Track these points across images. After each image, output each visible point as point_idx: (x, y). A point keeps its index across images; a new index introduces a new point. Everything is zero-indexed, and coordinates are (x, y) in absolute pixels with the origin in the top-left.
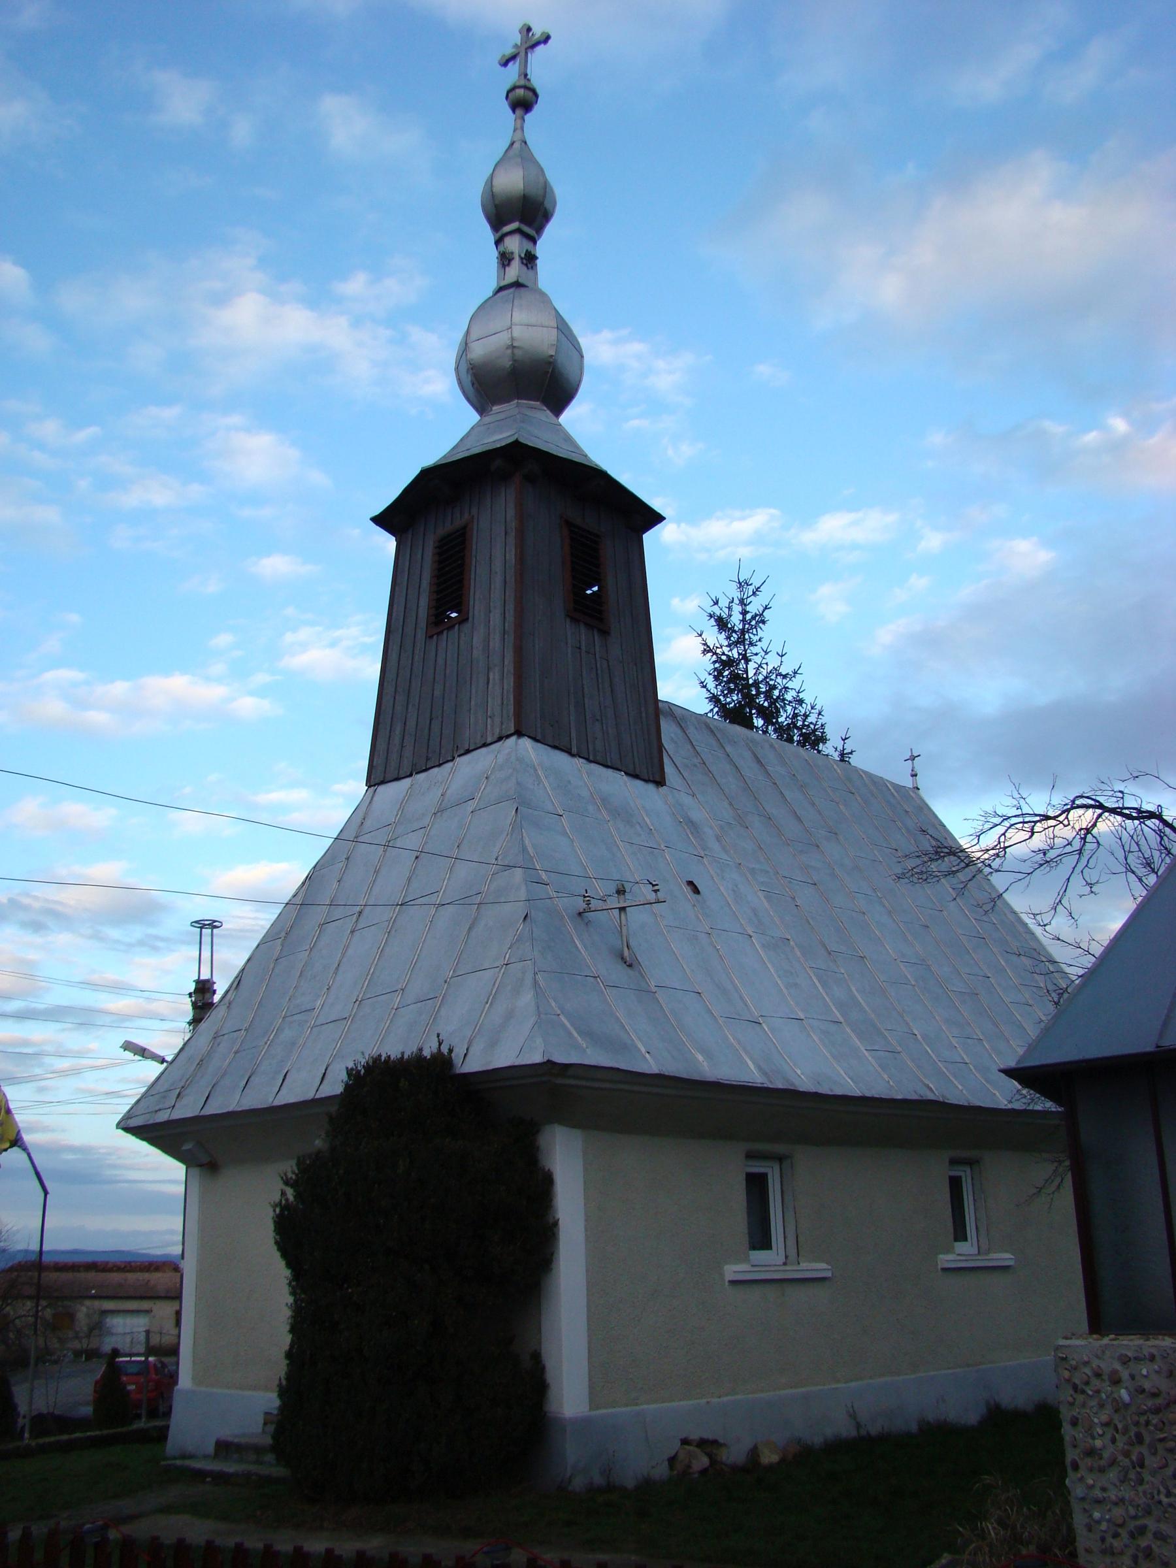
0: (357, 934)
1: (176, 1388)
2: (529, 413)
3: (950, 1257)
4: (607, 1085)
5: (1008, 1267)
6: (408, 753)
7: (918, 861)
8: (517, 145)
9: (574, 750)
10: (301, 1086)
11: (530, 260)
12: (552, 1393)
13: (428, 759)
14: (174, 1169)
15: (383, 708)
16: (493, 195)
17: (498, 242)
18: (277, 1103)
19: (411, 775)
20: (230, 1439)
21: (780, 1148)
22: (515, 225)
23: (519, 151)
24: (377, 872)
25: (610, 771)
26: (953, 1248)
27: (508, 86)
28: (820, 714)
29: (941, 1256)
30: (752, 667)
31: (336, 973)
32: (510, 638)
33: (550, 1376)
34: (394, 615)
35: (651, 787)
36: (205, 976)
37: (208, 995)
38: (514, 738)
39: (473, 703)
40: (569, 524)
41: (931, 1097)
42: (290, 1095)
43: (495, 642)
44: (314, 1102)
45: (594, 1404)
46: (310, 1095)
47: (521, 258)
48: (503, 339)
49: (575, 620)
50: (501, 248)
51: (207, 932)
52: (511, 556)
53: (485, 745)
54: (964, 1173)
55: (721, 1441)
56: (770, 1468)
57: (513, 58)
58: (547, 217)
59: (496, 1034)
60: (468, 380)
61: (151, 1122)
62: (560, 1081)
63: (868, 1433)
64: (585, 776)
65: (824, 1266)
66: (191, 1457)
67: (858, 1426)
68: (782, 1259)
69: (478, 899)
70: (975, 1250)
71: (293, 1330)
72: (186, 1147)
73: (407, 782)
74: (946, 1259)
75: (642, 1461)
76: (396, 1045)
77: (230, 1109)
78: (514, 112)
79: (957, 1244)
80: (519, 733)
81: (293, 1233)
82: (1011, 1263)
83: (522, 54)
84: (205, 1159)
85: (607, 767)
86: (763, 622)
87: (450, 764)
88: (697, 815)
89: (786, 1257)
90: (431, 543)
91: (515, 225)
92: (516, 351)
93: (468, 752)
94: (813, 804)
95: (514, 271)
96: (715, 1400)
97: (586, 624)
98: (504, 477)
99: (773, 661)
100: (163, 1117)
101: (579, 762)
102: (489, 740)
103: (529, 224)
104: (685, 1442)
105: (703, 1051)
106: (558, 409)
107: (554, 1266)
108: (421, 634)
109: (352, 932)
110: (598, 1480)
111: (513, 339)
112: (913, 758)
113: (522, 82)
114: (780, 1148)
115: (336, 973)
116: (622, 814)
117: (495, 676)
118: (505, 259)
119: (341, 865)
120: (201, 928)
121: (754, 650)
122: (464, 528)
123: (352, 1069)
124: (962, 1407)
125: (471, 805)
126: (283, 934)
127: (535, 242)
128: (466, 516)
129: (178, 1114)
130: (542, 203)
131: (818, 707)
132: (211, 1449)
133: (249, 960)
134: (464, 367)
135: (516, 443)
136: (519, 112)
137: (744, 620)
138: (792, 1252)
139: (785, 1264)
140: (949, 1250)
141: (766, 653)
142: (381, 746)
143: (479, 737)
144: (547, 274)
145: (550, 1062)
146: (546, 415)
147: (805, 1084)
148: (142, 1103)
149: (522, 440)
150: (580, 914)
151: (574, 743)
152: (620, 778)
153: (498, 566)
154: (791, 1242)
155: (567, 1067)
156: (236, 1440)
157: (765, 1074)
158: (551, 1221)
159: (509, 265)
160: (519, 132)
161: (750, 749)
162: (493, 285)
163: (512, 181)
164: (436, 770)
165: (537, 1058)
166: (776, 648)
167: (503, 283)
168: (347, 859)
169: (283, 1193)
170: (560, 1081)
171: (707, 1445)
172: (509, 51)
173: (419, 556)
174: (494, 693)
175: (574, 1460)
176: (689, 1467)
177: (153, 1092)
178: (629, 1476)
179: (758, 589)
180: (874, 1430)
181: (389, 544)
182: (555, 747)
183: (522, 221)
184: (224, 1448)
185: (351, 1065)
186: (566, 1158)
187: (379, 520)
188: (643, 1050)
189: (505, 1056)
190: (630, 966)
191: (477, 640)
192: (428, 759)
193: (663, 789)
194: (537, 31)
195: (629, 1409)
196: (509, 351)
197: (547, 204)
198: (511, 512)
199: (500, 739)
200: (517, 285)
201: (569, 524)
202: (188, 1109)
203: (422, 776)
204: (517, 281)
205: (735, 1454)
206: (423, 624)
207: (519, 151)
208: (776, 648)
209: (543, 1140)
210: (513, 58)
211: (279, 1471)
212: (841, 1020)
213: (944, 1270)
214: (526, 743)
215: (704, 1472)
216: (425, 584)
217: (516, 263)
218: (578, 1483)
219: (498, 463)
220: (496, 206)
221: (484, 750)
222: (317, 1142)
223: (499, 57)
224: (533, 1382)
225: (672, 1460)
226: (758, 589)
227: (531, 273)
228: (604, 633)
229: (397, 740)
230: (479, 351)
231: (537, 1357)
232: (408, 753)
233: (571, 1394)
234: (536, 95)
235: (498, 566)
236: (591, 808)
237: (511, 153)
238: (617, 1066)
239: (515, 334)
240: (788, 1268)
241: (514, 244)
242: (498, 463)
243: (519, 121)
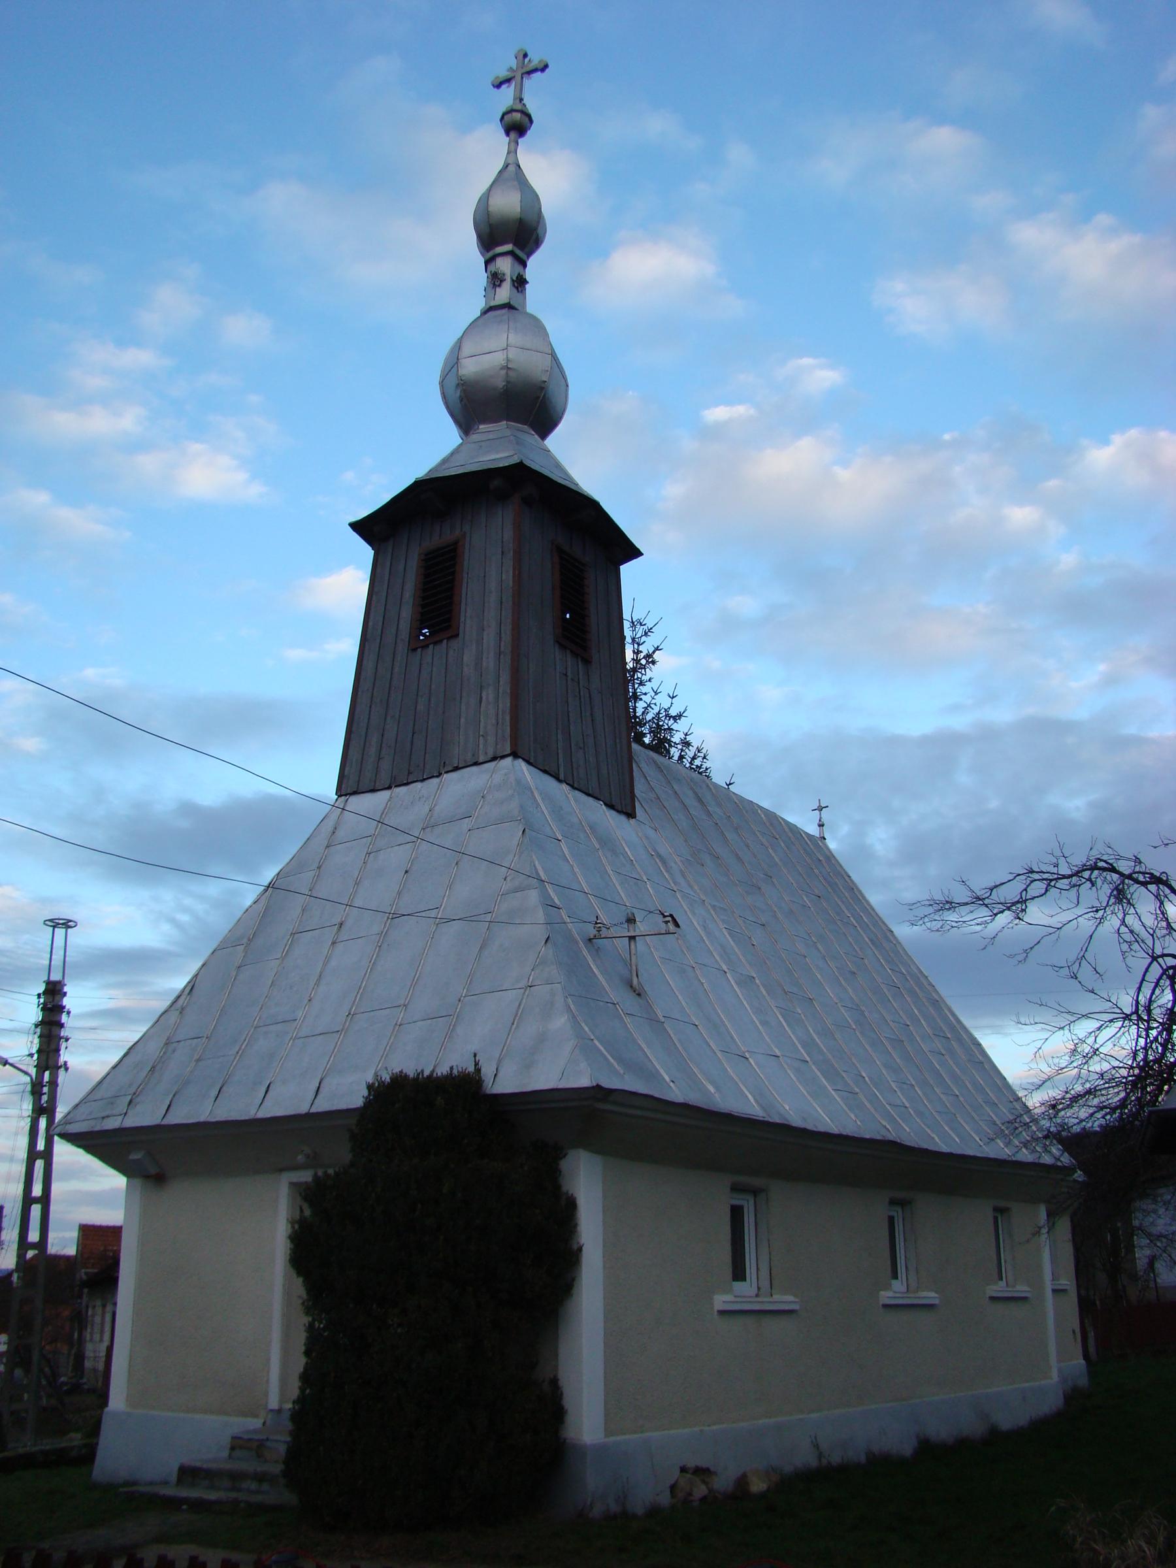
0: (340, 947)
1: (106, 1410)
2: (519, 434)
3: (890, 1294)
4: (639, 1113)
5: (791, 1312)
6: (385, 765)
7: (931, 910)
8: (512, 168)
9: (562, 777)
10: (289, 1098)
11: (520, 283)
12: (570, 1419)
13: (410, 773)
14: (117, 1181)
15: (356, 717)
16: (488, 214)
17: (487, 263)
18: (261, 1115)
19: (389, 788)
20: (198, 1464)
21: (756, 1182)
22: (508, 247)
23: (511, 174)
24: (357, 883)
25: (591, 800)
26: (890, 1285)
27: (503, 109)
28: (704, 758)
29: (882, 1293)
30: (640, 705)
31: (318, 983)
32: (507, 660)
33: (568, 1402)
34: (371, 624)
35: (623, 818)
36: (55, 977)
37: (57, 998)
38: (510, 759)
39: (463, 720)
40: (560, 550)
41: (891, 1138)
42: (274, 1108)
43: (489, 662)
44: (309, 1116)
45: (608, 1432)
46: (303, 1108)
47: (513, 280)
48: (498, 359)
49: (563, 647)
50: (492, 268)
51: (60, 932)
52: (508, 577)
53: (476, 764)
54: (897, 1213)
55: (712, 1469)
56: (763, 1496)
57: (508, 81)
58: (537, 243)
59: (533, 1052)
60: (455, 395)
61: (97, 1128)
62: (601, 1106)
63: (829, 1463)
64: (573, 802)
65: (933, 1294)
66: (135, 1483)
67: (820, 1456)
68: (754, 1290)
69: (488, 917)
70: (904, 1289)
71: (307, 1353)
72: (135, 1156)
73: (384, 795)
74: (886, 1296)
75: (649, 1489)
76: (412, 1059)
77: (202, 1119)
78: (507, 134)
79: (894, 1282)
80: (515, 755)
81: (308, 1252)
82: (937, 1302)
83: (518, 77)
84: (153, 1170)
85: (588, 795)
86: (654, 662)
87: (435, 781)
88: (665, 849)
89: (759, 1289)
90: (416, 556)
91: (508, 247)
92: (511, 373)
93: (456, 769)
94: (748, 846)
95: (504, 293)
96: (707, 1428)
97: (572, 651)
98: (502, 497)
99: (663, 701)
100: (112, 1124)
101: (564, 786)
102: (481, 760)
103: (522, 248)
104: (683, 1470)
105: (713, 1083)
106: (544, 435)
107: (575, 1291)
108: (402, 648)
109: (334, 943)
110: (614, 1508)
111: (508, 360)
112: (820, 809)
113: (519, 107)
114: (756, 1182)
115: (318, 983)
116: (608, 843)
117: (489, 694)
118: (496, 280)
119: (312, 873)
120: (54, 927)
121: (643, 689)
122: (456, 543)
123: (373, 1084)
124: (898, 1440)
125: (466, 824)
126: (245, 941)
127: (525, 266)
128: (457, 532)
129: (130, 1122)
130: (536, 229)
131: (704, 751)
132: (174, 1478)
133: (203, 965)
134: (452, 381)
135: (520, 466)
136: (513, 135)
137: (637, 661)
138: (765, 1283)
139: (757, 1296)
140: (887, 1287)
141: (656, 693)
142: (354, 755)
143: (470, 754)
144: (535, 300)
145: (598, 1087)
146: (532, 438)
147: (796, 1121)
148: (82, 1109)
149: (528, 463)
150: (590, 940)
151: (562, 769)
152: (600, 807)
153: (493, 585)
154: (764, 1273)
155: (611, 1091)
156: (205, 1466)
157: (765, 1111)
158: (575, 1247)
159: (499, 286)
160: (512, 154)
161: (692, 789)
162: (480, 304)
163: (508, 203)
164: (418, 785)
165: (584, 1082)
166: (667, 689)
167: (493, 304)
168: (319, 868)
169: (302, 1210)
170: (601, 1106)
171: (702, 1472)
172: (503, 74)
173: (401, 567)
174: (490, 710)
175: (593, 1487)
176: (690, 1494)
177: (91, 1097)
178: (638, 1506)
179: (650, 630)
180: (836, 1459)
181: (366, 553)
182: (545, 772)
183: (515, 244)
184: (188, 1474)
185: (370, 1079)
186: (587, 1182)
187: (357, 527)
188: (667, 1078)
189: (546, 1076)
190: (639, 995)
191: (468, 657)
192: (410, 773)
193: (632, 821)
194: (535, 59)
195: (636, 1436)
196: (503, 372)
197: (540, 231)
198: (508, 534)
199: (494, 759)
200: (508, 306)
201: (560, 550)
202: (146, 1115)
203: (403, 789)
204: (506, 304)
205: (723, 1482)
206: (405, 633)
207: (511, 174)
208: (667, 689)
209: (564, 1165)
210: (508, 81)
211: (289, 1498)
212: (808, 1059)
213: (885, 1306)
214: (521, 765)
215: (703, 1499)
216: (408, 595)
217: (507, 285)
218: (597, 1511)
219: (496, 483)
220: (490, 225)
221: (474, 769)
222: (300, 1157)
223: (492, 78)
224: (551, 1407)
225: (673, 1488)
226: (650, 630)
227: (519, 295)
228: (587, 662)
229: (372, 751)
230: (470, 368)
231: (555, 1383)
232: (385, 765)
233: (588, 1421)
234: (531, 121)
235: (493, 585)
236: (582, 835)
237: (506, 175)
238: (651, 1093)
239: (510, 356)
240: (759, 1299)
241: (505, 265)
242: (496, 483)
243: (513, 144)
